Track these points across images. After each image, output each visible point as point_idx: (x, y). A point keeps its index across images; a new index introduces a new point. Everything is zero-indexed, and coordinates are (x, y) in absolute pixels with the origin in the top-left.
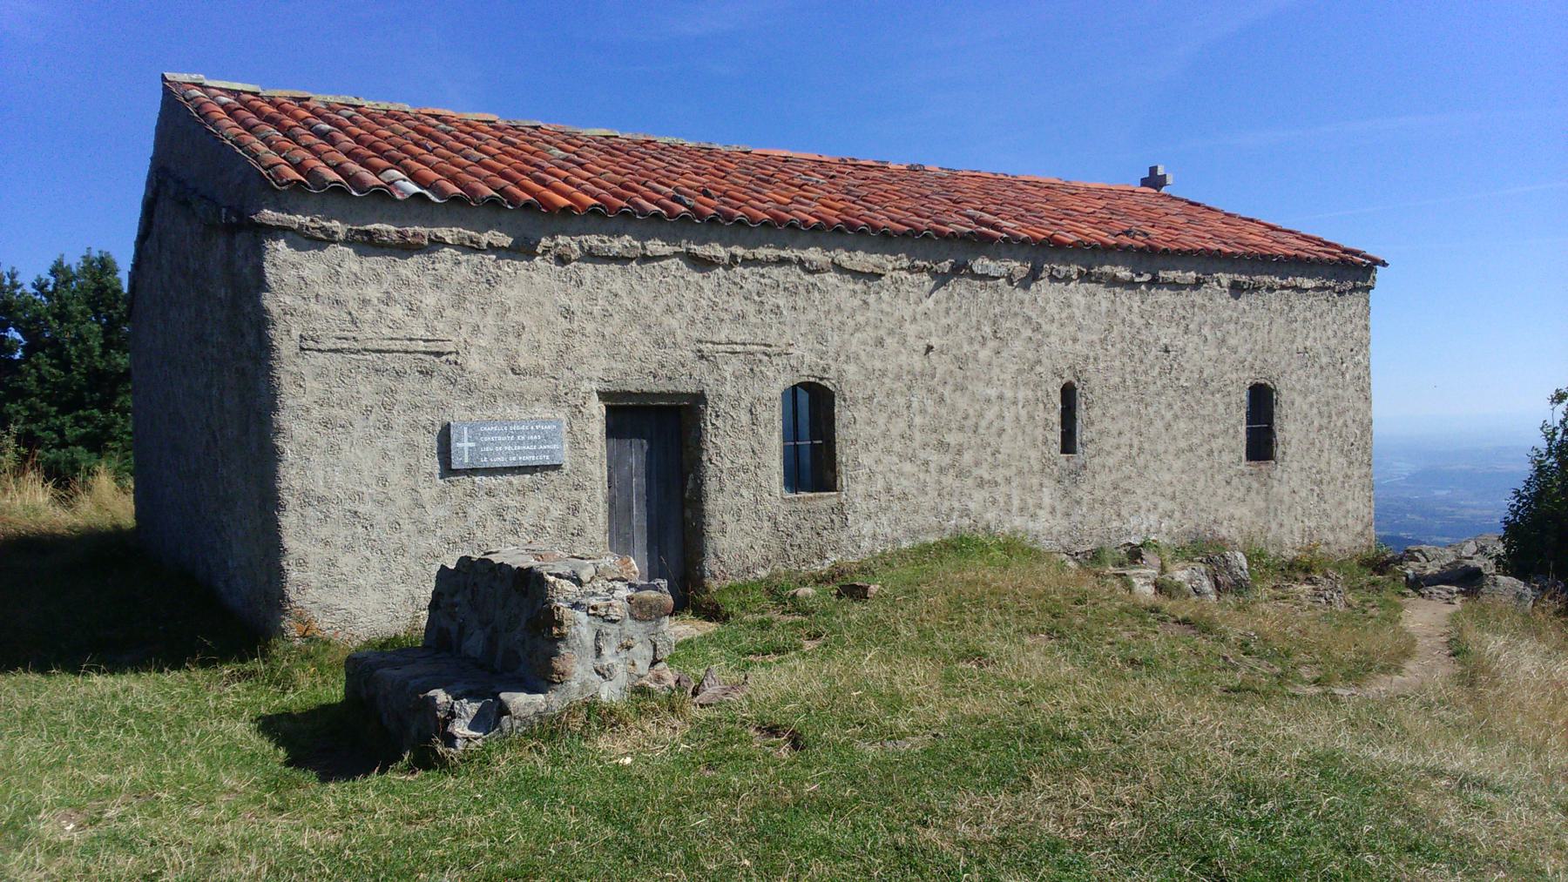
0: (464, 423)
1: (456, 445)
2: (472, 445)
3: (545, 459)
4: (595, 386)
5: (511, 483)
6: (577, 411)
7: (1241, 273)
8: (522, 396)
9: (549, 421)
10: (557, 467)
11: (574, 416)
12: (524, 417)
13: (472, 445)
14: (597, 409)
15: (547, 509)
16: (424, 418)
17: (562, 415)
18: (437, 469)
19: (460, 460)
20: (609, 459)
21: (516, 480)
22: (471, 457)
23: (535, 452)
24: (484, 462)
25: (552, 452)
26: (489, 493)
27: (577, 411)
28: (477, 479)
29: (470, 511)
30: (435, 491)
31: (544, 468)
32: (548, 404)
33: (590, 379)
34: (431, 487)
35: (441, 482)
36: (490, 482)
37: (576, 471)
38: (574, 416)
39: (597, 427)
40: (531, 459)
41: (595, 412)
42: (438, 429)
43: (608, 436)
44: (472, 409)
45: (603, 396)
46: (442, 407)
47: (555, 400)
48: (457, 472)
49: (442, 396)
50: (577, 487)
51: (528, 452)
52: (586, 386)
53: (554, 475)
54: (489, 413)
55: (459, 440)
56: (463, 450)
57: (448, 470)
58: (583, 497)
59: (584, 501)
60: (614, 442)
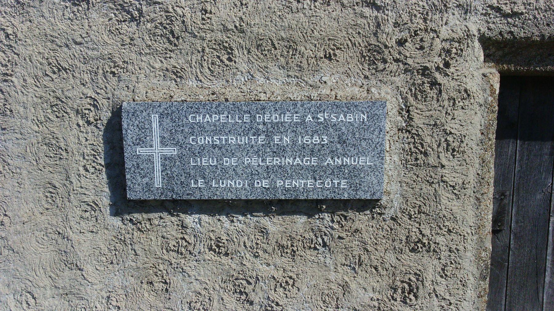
0: (150, 106)
1: (134, 152)
2: (172, 151)
3: (342, 188)
4: (475, 25)
5: (263, 231)
6: (427, 82)
7: (509, 63)
8: (291, 46)
9: (351, 106)
10: (368, 205)
11: (418, 93)
12: (296, 94)
13: (172, 151)
14: (478, 77)
15: (345, 287)
16: (76, 92)
17: (388, 93)
18: (105, 201)
19: (136, 192)
20: (501, 180)
21: (274, 224)
22: (168, 178)
23: (315, 173)
24: (198, 188)
25: (353, 173)
26: (217, 247)
27: (427, 82)
28: (190, 220)
29: (176, 280)
30: (102, 240)
31: (337, 206)
32: (355, 67)
33: (466, 10)
34: (97, 232)
35: (116, 222)
36: (223, 225)
37: (417, 212)
38: (418, 93)
39: (475, 121)
40: (304, 186)
41: (473, 84)
42: (106, 115)
43: (501, 135)
44: (178, 75)
45: (496, 49)
46: (115, 69)
47: (374, 57)
48: (143, 206)
49: (111, 45)
50: (416, 246)
51: (298, 171)
52: (452, 24)
53: (361, 220)
54: (218, 85)
55: (140, 142)
56: (152, 155)
57: (124, 204)
58: (430, 266)
59: (429, 275)
60: (514, 147)
